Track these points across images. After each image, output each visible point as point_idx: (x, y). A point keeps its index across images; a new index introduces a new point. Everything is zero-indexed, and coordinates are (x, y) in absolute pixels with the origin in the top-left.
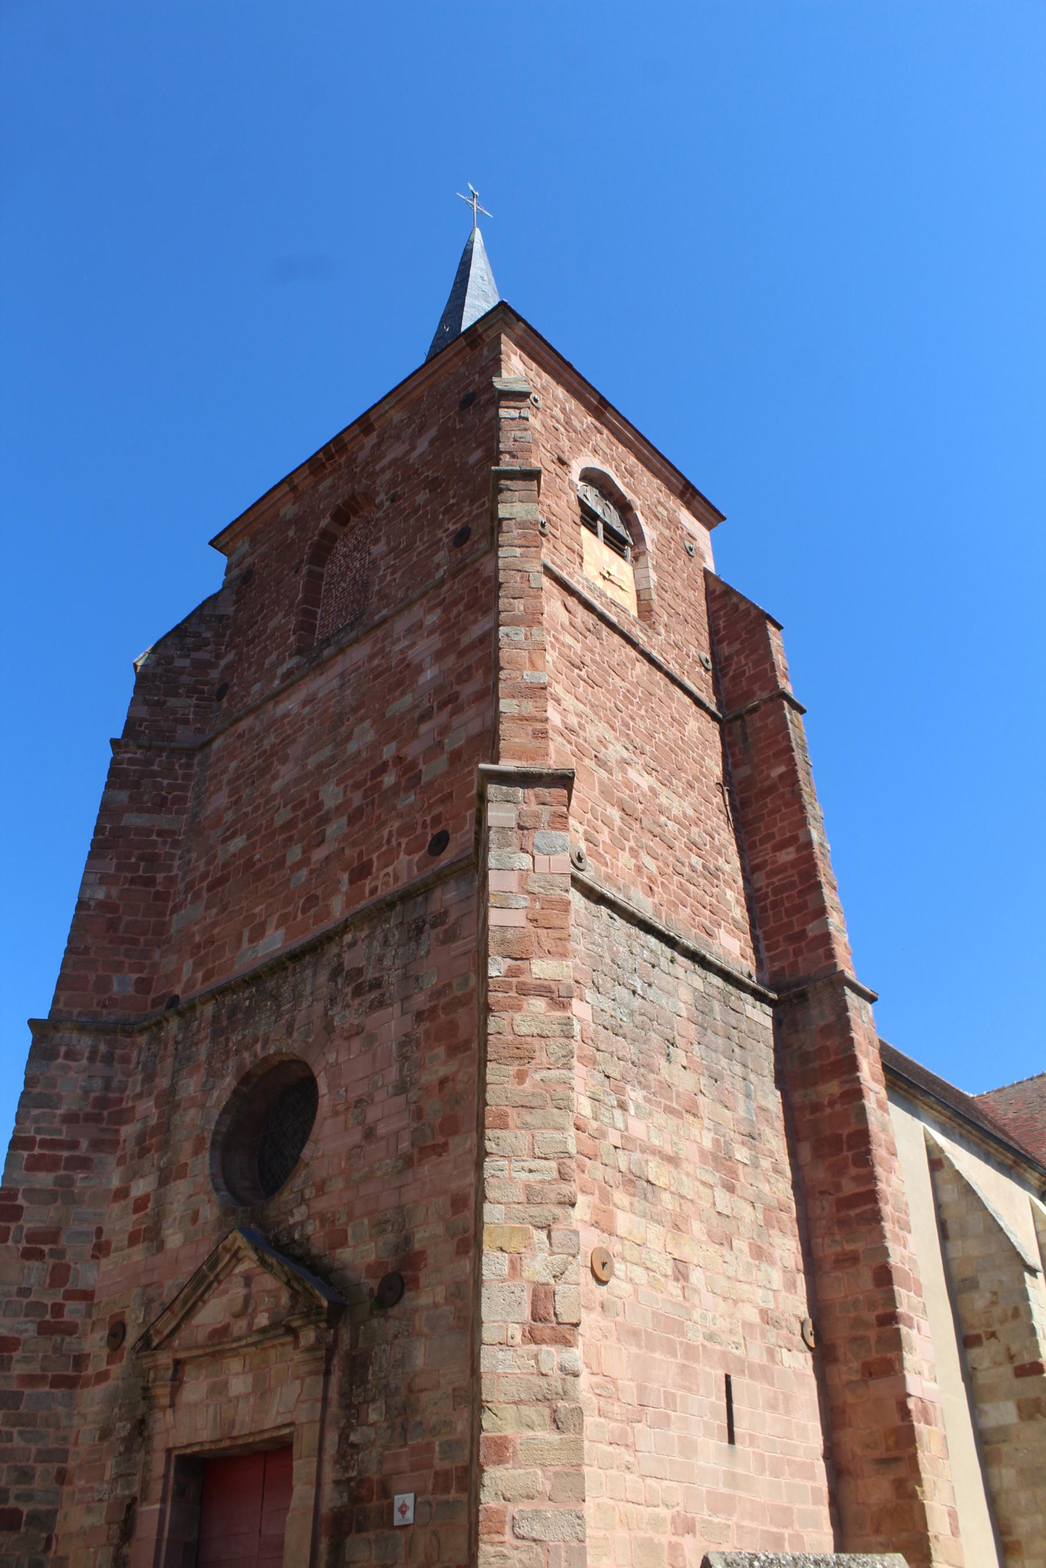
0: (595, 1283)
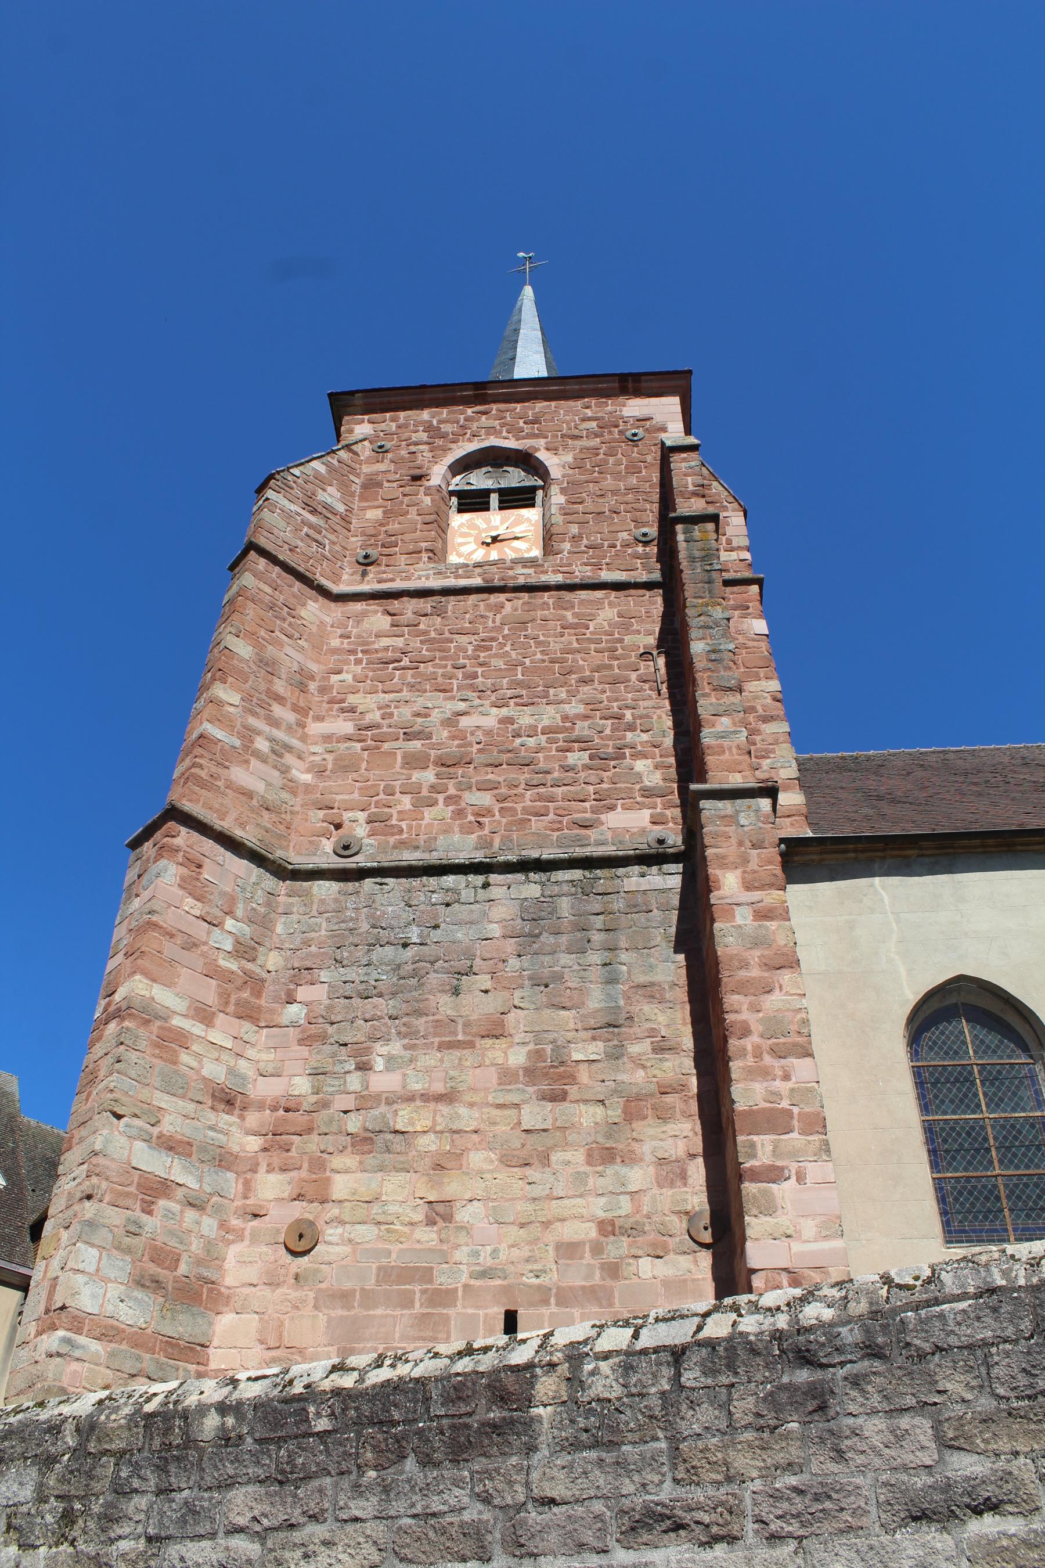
0: (290, 1257)
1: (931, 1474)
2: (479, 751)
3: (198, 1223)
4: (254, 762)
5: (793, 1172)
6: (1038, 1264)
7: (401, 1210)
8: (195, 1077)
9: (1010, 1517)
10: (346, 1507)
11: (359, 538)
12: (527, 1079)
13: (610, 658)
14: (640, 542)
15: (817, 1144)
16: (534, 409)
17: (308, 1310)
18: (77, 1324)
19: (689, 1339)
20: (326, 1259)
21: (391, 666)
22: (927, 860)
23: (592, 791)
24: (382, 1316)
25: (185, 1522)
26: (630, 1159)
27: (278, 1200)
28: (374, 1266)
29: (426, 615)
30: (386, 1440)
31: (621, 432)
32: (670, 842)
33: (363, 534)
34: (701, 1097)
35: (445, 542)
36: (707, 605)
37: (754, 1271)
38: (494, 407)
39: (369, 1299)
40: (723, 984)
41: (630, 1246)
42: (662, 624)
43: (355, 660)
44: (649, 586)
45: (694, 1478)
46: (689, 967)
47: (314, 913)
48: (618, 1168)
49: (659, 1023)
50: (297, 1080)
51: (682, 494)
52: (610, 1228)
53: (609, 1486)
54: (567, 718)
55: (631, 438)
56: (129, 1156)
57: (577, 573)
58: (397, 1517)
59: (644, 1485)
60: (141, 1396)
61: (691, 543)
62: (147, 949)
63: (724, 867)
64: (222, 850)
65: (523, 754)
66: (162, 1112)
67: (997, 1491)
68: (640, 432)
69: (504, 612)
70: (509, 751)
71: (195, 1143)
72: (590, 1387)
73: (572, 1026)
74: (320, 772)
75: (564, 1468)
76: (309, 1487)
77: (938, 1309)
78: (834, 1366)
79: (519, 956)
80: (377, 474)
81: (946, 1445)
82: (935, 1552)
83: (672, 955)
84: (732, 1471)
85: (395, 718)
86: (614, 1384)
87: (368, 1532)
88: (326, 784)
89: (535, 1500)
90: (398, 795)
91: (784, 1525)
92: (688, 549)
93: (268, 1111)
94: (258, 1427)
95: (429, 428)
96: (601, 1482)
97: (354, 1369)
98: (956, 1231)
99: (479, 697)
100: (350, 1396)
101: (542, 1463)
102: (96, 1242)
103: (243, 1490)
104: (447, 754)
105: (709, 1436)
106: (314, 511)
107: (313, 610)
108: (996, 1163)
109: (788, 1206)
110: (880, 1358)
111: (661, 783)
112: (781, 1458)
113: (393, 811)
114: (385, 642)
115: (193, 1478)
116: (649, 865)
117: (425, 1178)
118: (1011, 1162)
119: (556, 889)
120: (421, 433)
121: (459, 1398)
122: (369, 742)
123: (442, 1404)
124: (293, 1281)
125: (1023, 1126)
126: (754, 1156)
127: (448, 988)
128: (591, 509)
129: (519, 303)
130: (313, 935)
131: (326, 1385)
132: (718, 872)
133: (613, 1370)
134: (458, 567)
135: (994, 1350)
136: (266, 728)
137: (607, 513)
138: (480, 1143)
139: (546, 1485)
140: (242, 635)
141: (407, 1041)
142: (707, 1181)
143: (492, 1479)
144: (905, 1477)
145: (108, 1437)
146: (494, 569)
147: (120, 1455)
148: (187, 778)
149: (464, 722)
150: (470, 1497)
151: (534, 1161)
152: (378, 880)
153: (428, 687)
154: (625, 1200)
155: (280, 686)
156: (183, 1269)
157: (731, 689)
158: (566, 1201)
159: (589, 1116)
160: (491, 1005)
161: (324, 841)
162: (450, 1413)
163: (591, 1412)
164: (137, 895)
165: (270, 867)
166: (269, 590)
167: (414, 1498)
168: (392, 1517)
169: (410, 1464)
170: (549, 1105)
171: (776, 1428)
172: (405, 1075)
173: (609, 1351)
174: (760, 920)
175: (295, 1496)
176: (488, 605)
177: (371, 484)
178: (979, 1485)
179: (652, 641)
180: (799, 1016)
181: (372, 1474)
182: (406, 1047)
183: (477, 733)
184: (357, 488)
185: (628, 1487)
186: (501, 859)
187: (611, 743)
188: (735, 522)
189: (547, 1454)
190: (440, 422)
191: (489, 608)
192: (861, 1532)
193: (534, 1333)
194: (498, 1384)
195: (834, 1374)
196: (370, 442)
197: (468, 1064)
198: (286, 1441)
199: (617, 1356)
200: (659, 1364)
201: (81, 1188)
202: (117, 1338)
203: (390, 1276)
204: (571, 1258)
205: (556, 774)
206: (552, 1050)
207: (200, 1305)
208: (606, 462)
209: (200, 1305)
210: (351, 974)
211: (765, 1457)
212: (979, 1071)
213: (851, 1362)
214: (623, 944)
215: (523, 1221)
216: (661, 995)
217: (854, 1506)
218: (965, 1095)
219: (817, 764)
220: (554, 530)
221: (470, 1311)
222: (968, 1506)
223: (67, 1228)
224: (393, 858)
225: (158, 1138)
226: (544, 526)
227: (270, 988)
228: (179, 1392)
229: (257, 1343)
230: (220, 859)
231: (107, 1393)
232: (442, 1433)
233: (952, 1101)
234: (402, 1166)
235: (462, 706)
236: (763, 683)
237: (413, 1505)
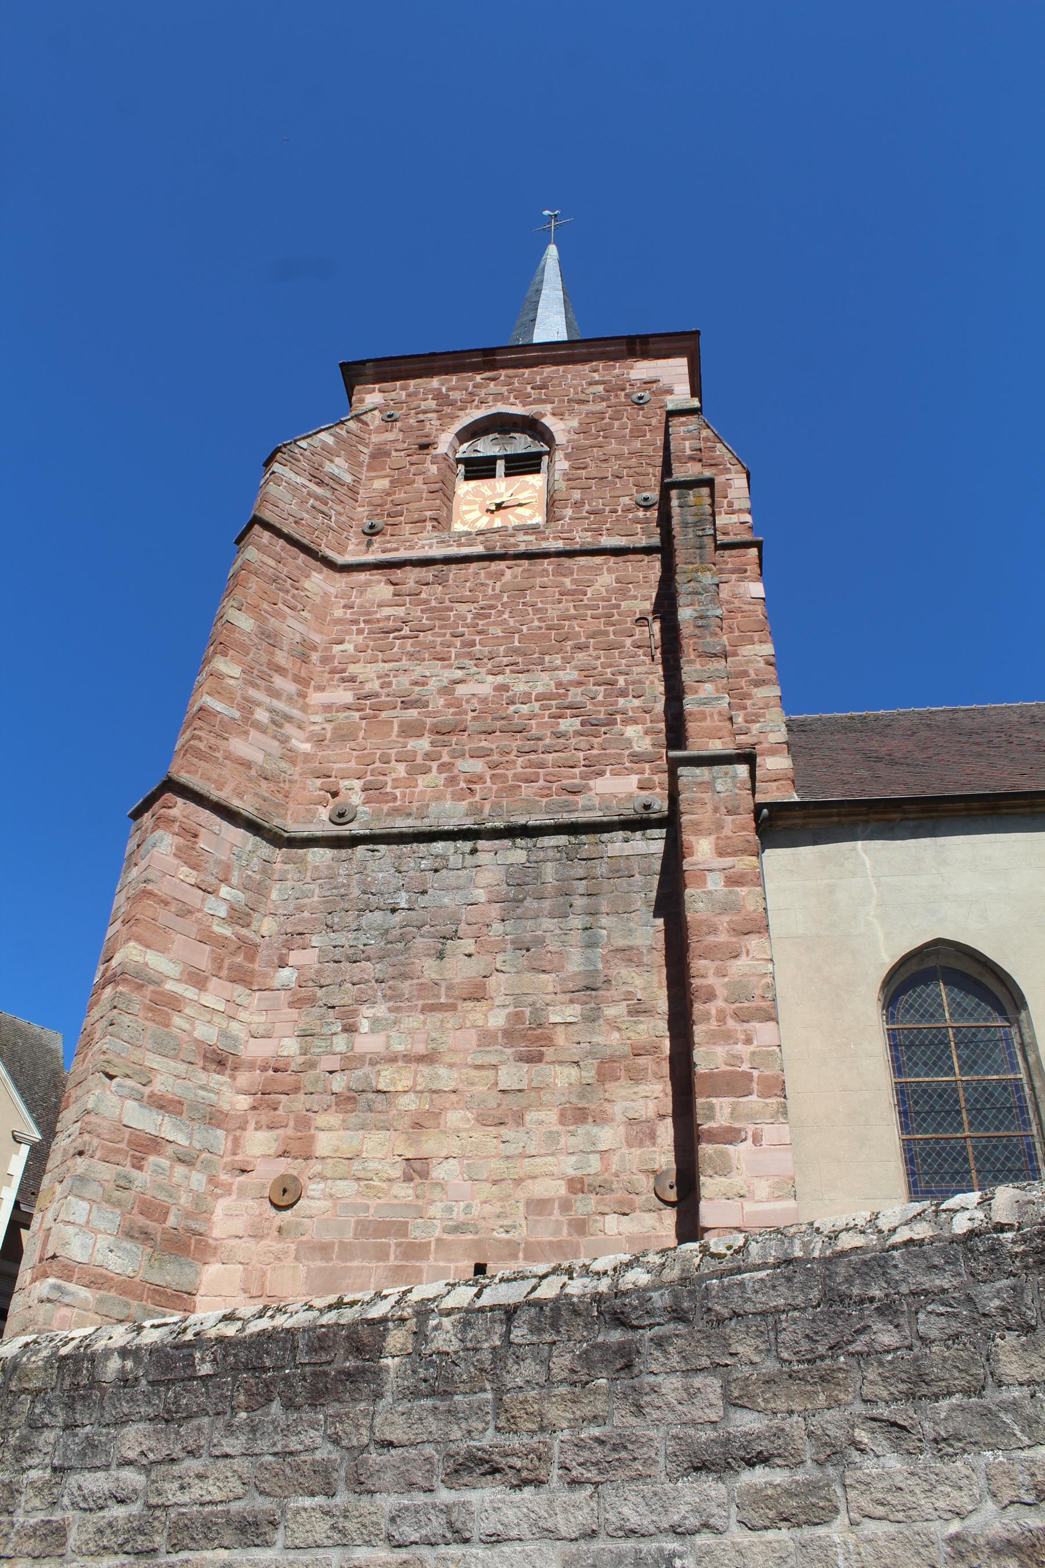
0: (274, 1211)
1: (715, 1429)
2: (474, 718)
3: (187, 1178)
4: (253, 733)
5: (750, 1134)
6: (836, 1237)
7: (380, 1167)
8: (187, 1039)
9: (778, 1469)
10: (219, 1444)
11: (366, 508)
12: (505, 1041)
13: (606, 624)
14: (641, 506)
15: (775, 1107)
16: (542, 373)
17: (289, 1262)
18: (68, 1272)
19: (522, 1299)
20: (308, 1213)
21: (392, 635)
22: (911, 824)
23: (582, 758)
24: (358, 1268)
25: (85, 1455)
26: (602, 1119)
27: (264, 1156)
28: (353, 1220)
29: (427, 584)
30: (257, 1384)
31: (627, 396)
32: (656, 807)
33: (370, 504)
34: (673, 1059)
35: (450, 510)
36: (697, 571)
37: (707, 1230)
38: (503, 373)
39: (346, 1251)
40: (691, 949)
41: (597, 1203)
42: (659, 589)
43: (357, 630)
44: (648, 551)
45: (513, 1427)
46: (667, 931)
48: (589, 1128)
49: (636, 987)
50: (286, 1041)
51: (679, 459)
54: (561, 685)
55: (637, 401)
56: (120, 1114)
57: (578, 539)
58: (260, 1455)
59: (469, 1432)
60: (61, 1340)
62: (142, 917)
63: (698, 833)
64: (218, 819)
65: (516, 721)
67: (770, 1445)
68: (647, 395)
69: (504, 579)
70: (503, 718)
71: (186, 1101)
72: (432, 1341)
73: (551, 989)
74: (319, 741)
75: (403, 1414)
77: (739, 1277)
78: (643, 1328)
79: (503, 920)
81: (732, 1403)
82: (708, 1499)
83: (651, 919)
84: (546, 1421)
85: (394, 687)
86: (453, 1338)
87: (235, 1467)
88: (325, 753)
89: (377, 1443)
90: (393, 763)
91: (584, 1472)
92: (681, 514)
93: (258, 1072)
94: (152, 1370)
95: (438, 396)
96: (434, 1428)
97: (239, 1319)
98: (922, 1192)
99: (476, 665)
100: (230, 1344)
102: (87, 1196)
103: (135, 1427)
104: (441, 722)
105: (529, 1389)
106: (321, 483)
107: (317, 581)
108: (966, 1125)
109: (743, 1166)
110: (684, 1322)
111: (650, 748)
112: (588, 1411)
114: (387, 611)
116: (633, 831)
117: (404, 1136)
118: (981, 1124)
120: (430, 401)
121: (322, 1348)
122: (368, 711)
125: (995, 1089)
126: (711, 1118)
127: (433, 952)
128: (595, 474)
129: (542, 263)
130: (306, 901)
131: (212, 1333)
132: (692, 838)
133: (454, 1326)
135: (783, 1317)
136: (267, 700)
140: (244, 608)
141: (392, 1003)
142: (675, 1141)
143: (342, 1422)
144: (692, 1431)
146: (496, 537)
147: (36, 1393)
148: (187, 750)
149: (461, 690)
150: (323, 1438)
151: (509, 1120)
152: (370, 847)
153: (427, 656)
155: (281, 658)
156: (172, 1221)
157: (715, 655)
158: (538, 1160)
159: (563, 1077)
160: (471, 969)
161: (321, 808)
162: (313, 1361)
164: (136, 865)
166: (272, 563)
167: (276, 1438)
168: (256, 1455)
170: (526, 1067)
171: (587, 1383)
172: (388, 1036)
174: (731, 886)
175: (178, 1433)
177: (380, 454)
178: (754, 1440)
179: (648, 606)
180: (764, 981)
181: (243, 1415)
182: (391, 1010)
184: (365, 458)
185: (456, 1433)
186: (489, 825)
187: (603, 709)
188: (738, 483)
189: (391, 1401)
190: (449, 389)
191: (490, 576)
192: (648, 1480)
193: (396, 1290)
195: (642, 1335)
196: (380, 411)
197: (449, 1026)
198: (174, 1384)
200: (493, 1321)
202: (105, 1285)
203: (367, 1229)
204: (540, 1214)
205: (547, 741)
206: (531, 1012)
207: (188, 1256)
208: (611, 426)
210: (341, 938)
211: (575, 1409)
212: (954, 1034)
213: (659, 1324)
214: (604, 909)
215: (496, 1178)
217: (646, 1456)
218: (939, 1058)
219: (824, 725)
220: (557, 496)
221: (442, 1264)
222: (743, 1459)
223: (61, 1182)
224: (383, 825)
225: (150, 1097)
226: (548, 492)
227: (263, 953)
229: (241, 1292)
230: (216, 829)
231: (34, 1336)
232: (304, 1379)
233: (925, 1064)
234: (382, 1124)
235: (459, 674)
236: (757, 647)
237: (274, 1444)
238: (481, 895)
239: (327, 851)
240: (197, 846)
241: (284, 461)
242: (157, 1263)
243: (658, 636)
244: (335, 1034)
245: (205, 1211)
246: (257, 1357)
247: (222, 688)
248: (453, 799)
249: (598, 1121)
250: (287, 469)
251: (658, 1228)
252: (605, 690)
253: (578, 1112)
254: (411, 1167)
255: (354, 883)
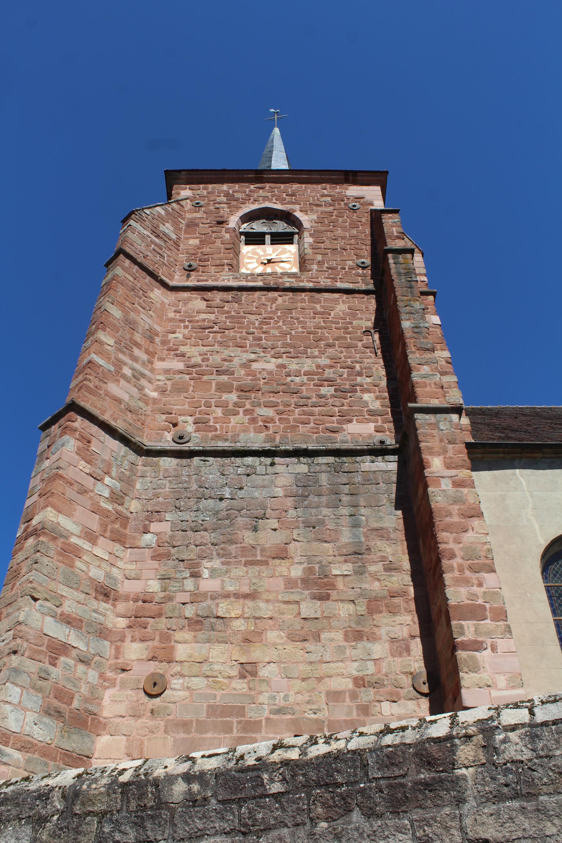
0: (147, 698)
2: (265, 383)
4: (122, 381)
5: (489, 645)
7: (222, 668)
8: (85, 577)
11: (185, 255)
15: (503, 627)
16: (292, 188)
17: (160, 734)
20: (172, 699)
21: (207, 331)
23: (337, 411)
24: (211, 738)
26: (373, 638)
28: (205, 705)
29: (228, 302)
35: (238, 261)
36: (410, 301)
38: (268, 185)
39: (202, 726)
42: (376, 315)
43: (184, 326)
44: (367, 292)
46: (404, 519)
47: (162, 477)
48: (365, 643)
49: (387, 553)
50: (151, 582)
52: (361, 683)
53: (534, 829)
55: (352, 208)
56: (42, 626)
57: (322, 283)
61: (398, 265)
62: (56, 491)
63: (432, 454)
65: (292, 386)
66: (64, 599)
68: (357, 204)
70: (284, 384)
71: (84, 620)
73: (331, 553)
74: (163, 391)
75: (491, 815)
76: (270, 836)
79: (296, 508)
80: (196, 218)
83: (394, 511)
85: (211, 361)
88: (167, 399)
90: (213, 407)
93: (131, 602)
94: (221, 791)
95: (227, 195)
96: (527, 825)
99: (263, 352)
100: (297, 766)
101: (472, 811)
102: (19, 683)
104: (244, 384)
106: (158, 236)
107: (158, 294)
109: (487, 666)
111: (380, 408)
113: (211, 417)
114: (203, 316)
115: (167, 831)
116: (377, 456)
117: (238, 648)
119: (318, 468)
121: (393, 764)
122: (194, 375)
123: (378, 769)
124: (150, 714)
126: (463, 634)
127: (250, 527)
128: (329, 246)
129: (271, 137)
130: (160, 490)
133: (521, 739)
134: (247, 275)
136: (130, 362)
137: (339, 249)
138: (273, 626)
139: (479, 829)
140: (115, 303)
141: (223, 559)
143: (430, 826)
145: (91, 801)
146: (270, 278)
150: (412, 840)
151: (310, 638)
152: (203, 458)
153: (231, 344)
154: (370, 664)
155: (138, 337)
156: (76, 704)
157: (428, 350)
158: (332, 665)
160: (279, 538)
161: (166, 433)
162: (386, 775)
163: (507, 771)
164: (47, 458)
165: (132, 447)
166: (131, 279)
169: (356, 816)
170: (319, 603)
173: (515, 724)
174: (457, 487)
176: (267, 298)
177: (192, 225)
179: (370, 324)
180: (485, 547)
181: (324, 825)
183: (263, 373)
186: (282, 448)
187: (348, 383)
189: (475, 804)
190: (234, 192)
191: (268, 300)
194: (424, 752)
196: (191, 201)
197: (264, 575)
198: (245, 802)
199: (523, 728)
201: (9, 646)
202: (32, 750)
204: (337, 702)
205: (314, 400)
206: (319, 568)
207: (87, 729)
209: (87, 729)
210: (186, 516)
214: (362, 503)
215: (304, 677)
216: (388, 535)
220: (307, 257)
225: (61, 615)
226: (300, 255)
227: (132, 523)
228: (146, 767)
229: (125, 756)
230: (102, 439)
232: (381, 791)
234: (222, 639)
235: (253, 356)
238: (280, 492)
239: (173, 459)
240: (90, 449)
241: (136, 220)
242: (66, 734)
243: (378, 342)
244: (186, 578)
245: (98, 698)
246: (327, 775)
247: (103, 350)
248: (255, 432)
249: (371, 639)
250: (138, 224)
251: (417, 711)
252: (348, 371)
253: (356, 633)
254: (244, 668)
255: (193, 480)
